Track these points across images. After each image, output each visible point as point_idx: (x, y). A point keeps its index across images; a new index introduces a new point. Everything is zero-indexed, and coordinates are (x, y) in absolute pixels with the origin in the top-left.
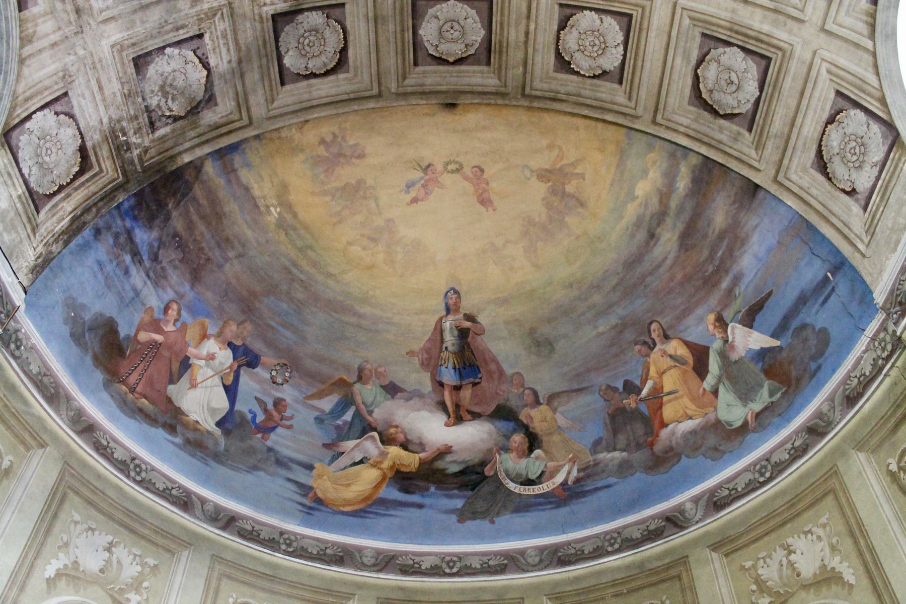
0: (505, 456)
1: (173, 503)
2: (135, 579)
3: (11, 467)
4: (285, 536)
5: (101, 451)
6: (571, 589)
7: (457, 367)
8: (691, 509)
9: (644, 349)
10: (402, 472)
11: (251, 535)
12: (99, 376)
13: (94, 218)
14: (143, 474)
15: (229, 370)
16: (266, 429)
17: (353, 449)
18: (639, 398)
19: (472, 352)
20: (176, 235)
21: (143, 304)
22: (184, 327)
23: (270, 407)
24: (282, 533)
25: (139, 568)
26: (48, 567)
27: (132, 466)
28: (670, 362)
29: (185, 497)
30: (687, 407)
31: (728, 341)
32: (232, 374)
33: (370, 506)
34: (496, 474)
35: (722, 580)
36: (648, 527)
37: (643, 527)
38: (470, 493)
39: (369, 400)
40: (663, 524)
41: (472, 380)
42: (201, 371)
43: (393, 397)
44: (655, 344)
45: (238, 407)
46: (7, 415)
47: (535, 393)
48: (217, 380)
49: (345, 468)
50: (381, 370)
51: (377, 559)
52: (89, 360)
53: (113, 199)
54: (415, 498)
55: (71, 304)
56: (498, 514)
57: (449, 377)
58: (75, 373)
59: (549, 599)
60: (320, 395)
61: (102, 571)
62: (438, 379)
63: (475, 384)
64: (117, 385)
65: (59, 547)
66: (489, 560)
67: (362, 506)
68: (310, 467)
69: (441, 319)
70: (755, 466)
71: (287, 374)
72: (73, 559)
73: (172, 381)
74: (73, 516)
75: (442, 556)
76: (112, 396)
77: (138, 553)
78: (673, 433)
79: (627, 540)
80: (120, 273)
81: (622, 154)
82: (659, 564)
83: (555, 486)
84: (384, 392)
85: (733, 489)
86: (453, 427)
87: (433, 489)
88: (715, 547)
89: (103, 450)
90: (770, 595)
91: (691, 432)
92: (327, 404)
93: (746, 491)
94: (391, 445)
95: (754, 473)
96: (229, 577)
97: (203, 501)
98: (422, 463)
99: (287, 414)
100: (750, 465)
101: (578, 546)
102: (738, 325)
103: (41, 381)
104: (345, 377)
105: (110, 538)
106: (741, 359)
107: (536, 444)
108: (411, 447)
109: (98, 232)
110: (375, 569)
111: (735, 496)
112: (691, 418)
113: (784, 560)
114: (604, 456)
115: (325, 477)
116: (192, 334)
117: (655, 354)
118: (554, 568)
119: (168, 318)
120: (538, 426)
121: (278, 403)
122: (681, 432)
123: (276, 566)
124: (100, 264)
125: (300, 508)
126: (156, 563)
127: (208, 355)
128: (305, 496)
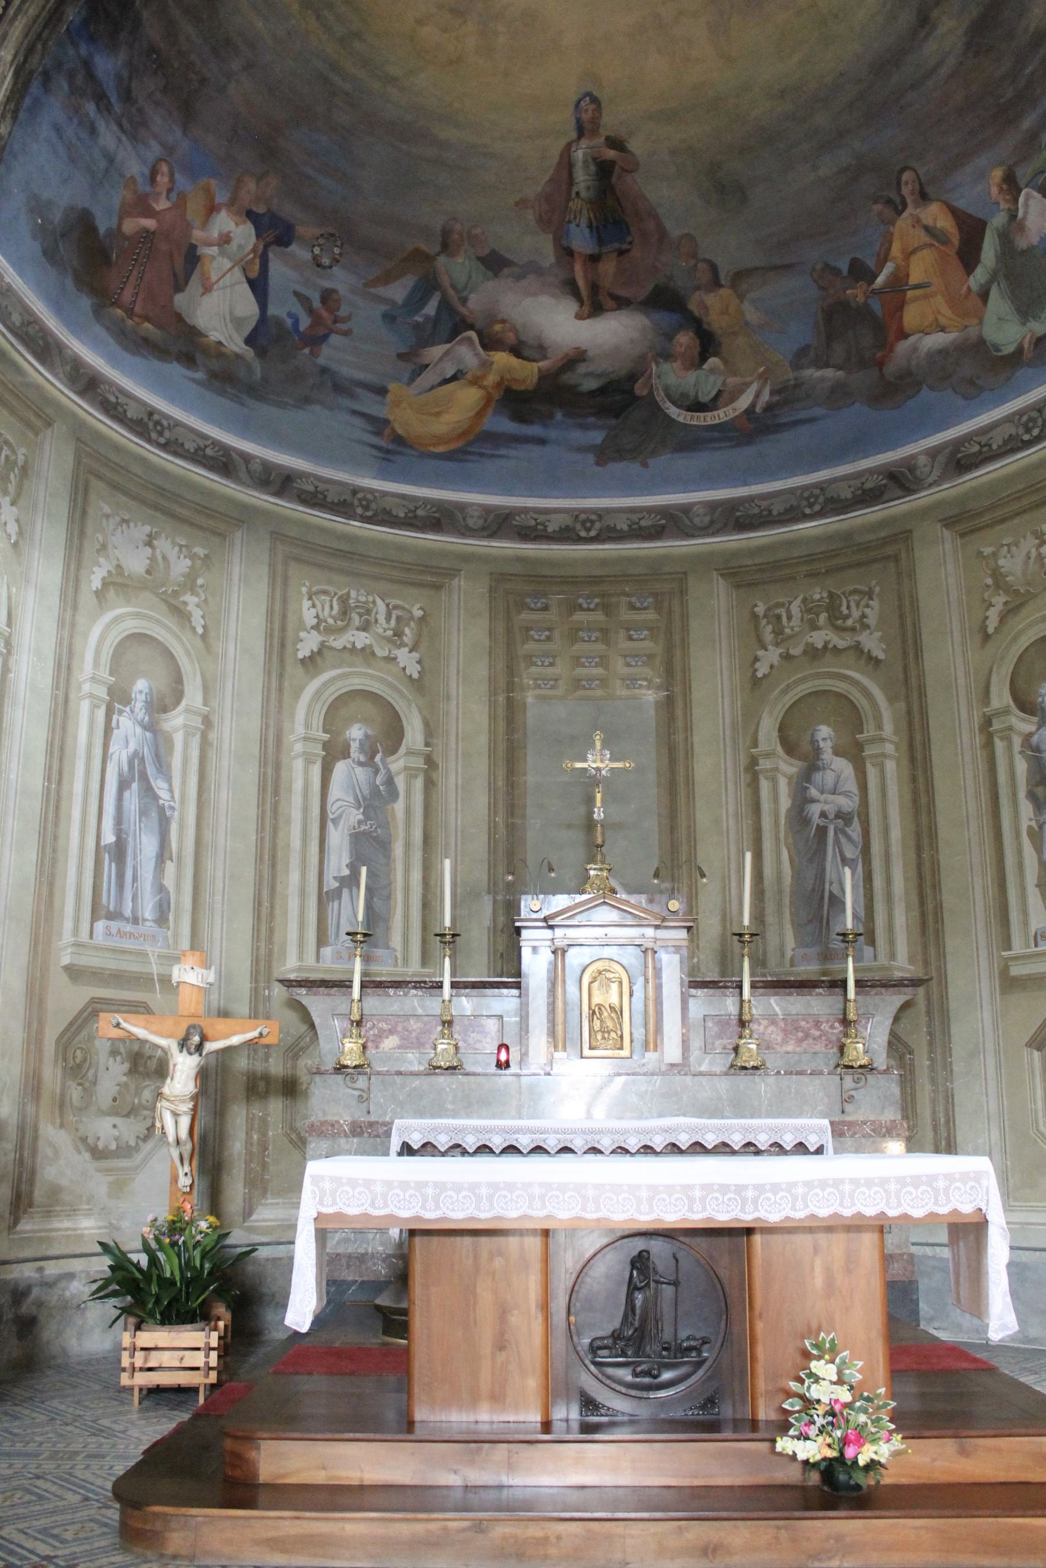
0: (666, 366)
1: (211, 468)
2: (187, 576)
3: (26, 462)
4: (360, 495)
5: (112, 413)
6: (749, 562)
7: (595, 224)
8: (925, 466)
9: (888, 212)
10: (516, 392)
11: (315, 499)
12: (86, 303)
13: (41, 60)
14: (167, 434)
15: (252, 256)
16: (315, 340)
17: (441, 359)
18: (870, 289)
19: (617, 200)
20: (152, 49)
21: (121, 175)
22: (182, 198)
23: (317, 304)
24: (355, 491)
25: (188, 562)
26: (93, 577)
27: (151, 425)
28: (925, 238)
29: (223, 456)
30: (939, 313)
31: (1016, 216)
32: (257, 261)
33: (471, 443)
34: (651, 393)
35: (950, 567)
36: (863, 484)
37: (857, 483)
38: (613, 422)
39: (461, 279)
40: (884, 482)
41: (616, 245)
42: (215, 264)
43: (496, 275)
44: (905, 206)
45: (272, 310)
46: (7, 396)
47: (714, 268)
48: (238, 274)
49: (432, 388)
50: (477, 231)
51: (486, 520)
52: (69, 282)
53: (60, 20)
54: (534, 430)
55: (37, 207)
56: (654, 453)
57: (581, 240)
58: (58, 308)
59: (721, 575)
60: (387, 278)
61: (148, 572)
62: (564, 243)
63: (621, 253)
64: (111, 310)
65: (98, 551)
66: (640, 519)
67: (459, 444)
68: (382, 391)
69: (569, 146)
70: (1021, 416)
71: (337, 250)
72: (115, 562)
73: (179, 288)
74: (101, 509)
75: (576, 514)
76: (107, 329)
77: (183, 543)
78: (915, 349)
79: (832, 500)
80: (84, 135)
81: (810, 922)
82: (872, 537)
83: (737, 413)
84: (482, 268)
85: (985, 445)
86: (587, 321)
87: (559, 416)
88: (948, 523)
89: (113, 409)
90: (1007, 592)
91: (940, 352)
92: (398, 291)
93: (1003, 450)
94: (496, 350)
95: (1017, 427)
96: (297, 559)
97: (247, 458)
98: (543, 376)
99: (342, 312)
100: (1014, 414)
101: (764, 504)
102: (1035, 194)
103: (27, 333)
104: (423, 247)
105: (147, 529)
106: (1031, 249)
107: (711, 350)
108: (527, 352)
109: (47, 77)
110: (485, 534)
111: (987, 455)
112: (943, 330)
113: (1033, 550)
114: (812, 374)
115: (404, 405)
116: (194, 208)
117: (903, 223)
118: (730, 534)
119: (158, 189)
120: (716, 322)
121: (328, 296)
122: (925, 350)
123: (353, 539)
124: (57, 129)
125: (375, 452)
126: (206, 552)
127: (221, 235)
128: (378, 433)
